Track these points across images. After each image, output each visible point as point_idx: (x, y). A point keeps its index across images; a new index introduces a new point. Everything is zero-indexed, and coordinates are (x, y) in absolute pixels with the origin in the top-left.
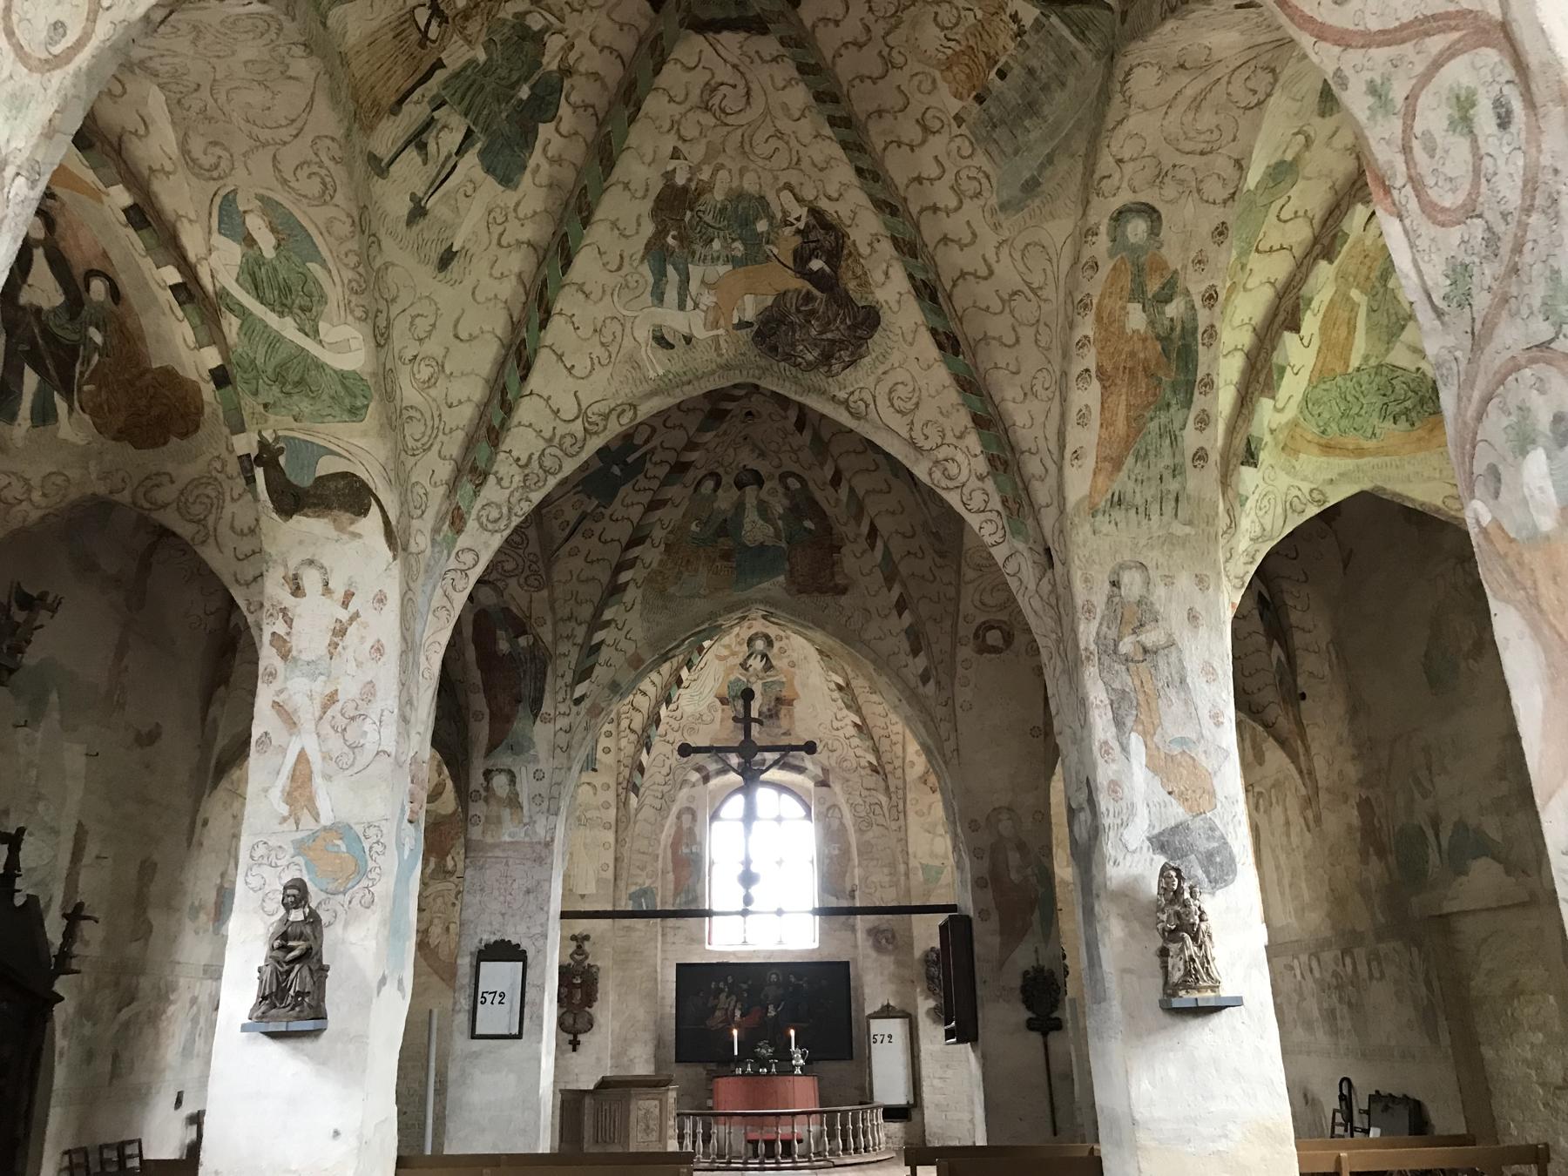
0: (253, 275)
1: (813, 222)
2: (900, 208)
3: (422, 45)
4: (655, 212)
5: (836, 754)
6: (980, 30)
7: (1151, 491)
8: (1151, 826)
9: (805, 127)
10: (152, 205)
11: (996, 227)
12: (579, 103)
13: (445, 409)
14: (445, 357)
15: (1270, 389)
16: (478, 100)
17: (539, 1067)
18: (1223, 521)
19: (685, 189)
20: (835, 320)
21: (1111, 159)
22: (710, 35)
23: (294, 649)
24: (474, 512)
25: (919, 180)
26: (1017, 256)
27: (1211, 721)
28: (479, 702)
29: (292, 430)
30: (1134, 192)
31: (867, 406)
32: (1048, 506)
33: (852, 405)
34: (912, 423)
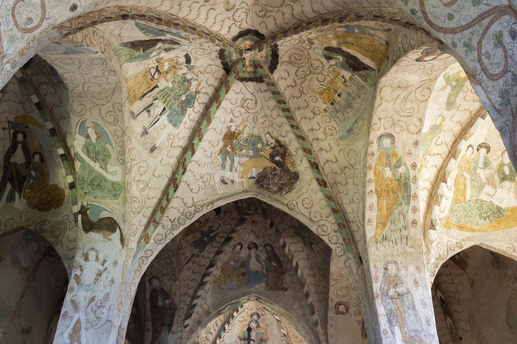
0: (87, 149)
1: (277, 144)
2: (306, 139)
3: (152, 80)
4: (224, 139)
6: (332, 82)
7: (397, 235)
9: (275, 113)
10: (59, 129)
11: (339, 145)
12: (201, 102)
13: (147, 200)
15: (438, 202)
16: (168, 99)
18: (425, 250)
19: (234, 133)
22: (245, 83)
23: (82, 280)
24: (153, 237)
25: (312, 129)
26: (346, 154)
28: (149, 325)
29: (93, 202)
30: (385, 129)
31: (294, 206)
32: (360, 241)
33: (289, 205)
34: (310, 212)
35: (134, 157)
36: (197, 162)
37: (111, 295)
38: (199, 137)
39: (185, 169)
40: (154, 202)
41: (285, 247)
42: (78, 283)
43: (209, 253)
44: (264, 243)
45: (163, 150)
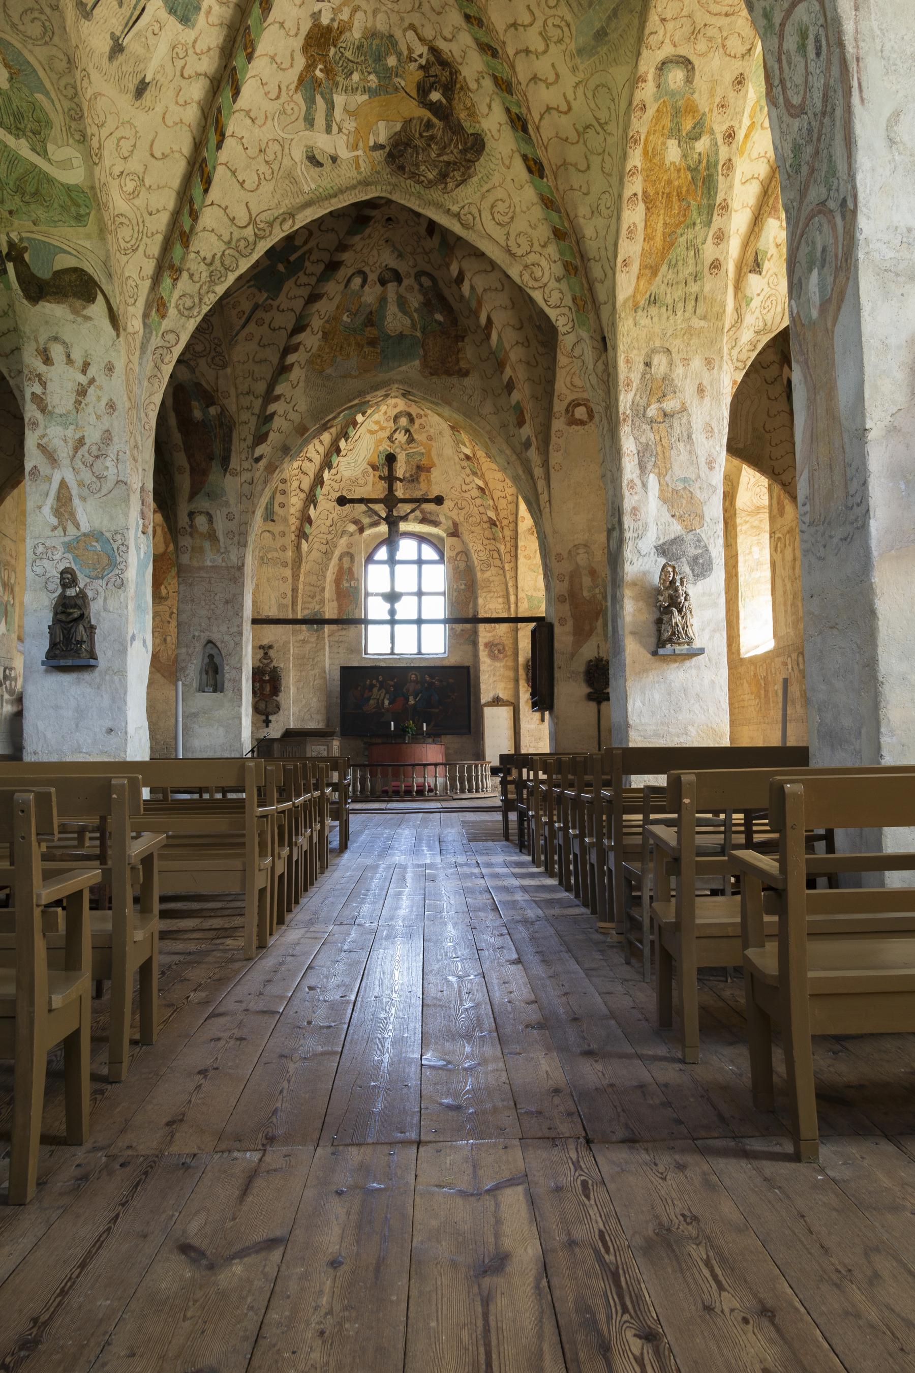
1: (432, 59)
4: (305, 49)
5: (464, 512)
7: (678, 293)
8: (658, 538)
11: (574, 69)
14: (144, 172)
17: (241, 723)
19: (329, 29)
20: (450, 145)
21: (657, 18)
24: (173, 302)
26: (590, 95)
27: (707, 467)
28: (181, 459)
29: (32, 232)
30: (675, 46)
31: (474, 218)
32: (605, 303)
34: (508, 234)
35: (102, 118)
36: (248, 113)
37: (114, 433)
38: (246, 49)
39: (223, 135)
40: (162, 221)
41: (462, 281)
42: (43, 410)
43: (291, 299)
44: (416, 270)
45: (164, 89)
